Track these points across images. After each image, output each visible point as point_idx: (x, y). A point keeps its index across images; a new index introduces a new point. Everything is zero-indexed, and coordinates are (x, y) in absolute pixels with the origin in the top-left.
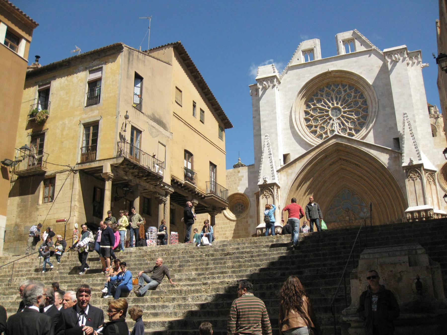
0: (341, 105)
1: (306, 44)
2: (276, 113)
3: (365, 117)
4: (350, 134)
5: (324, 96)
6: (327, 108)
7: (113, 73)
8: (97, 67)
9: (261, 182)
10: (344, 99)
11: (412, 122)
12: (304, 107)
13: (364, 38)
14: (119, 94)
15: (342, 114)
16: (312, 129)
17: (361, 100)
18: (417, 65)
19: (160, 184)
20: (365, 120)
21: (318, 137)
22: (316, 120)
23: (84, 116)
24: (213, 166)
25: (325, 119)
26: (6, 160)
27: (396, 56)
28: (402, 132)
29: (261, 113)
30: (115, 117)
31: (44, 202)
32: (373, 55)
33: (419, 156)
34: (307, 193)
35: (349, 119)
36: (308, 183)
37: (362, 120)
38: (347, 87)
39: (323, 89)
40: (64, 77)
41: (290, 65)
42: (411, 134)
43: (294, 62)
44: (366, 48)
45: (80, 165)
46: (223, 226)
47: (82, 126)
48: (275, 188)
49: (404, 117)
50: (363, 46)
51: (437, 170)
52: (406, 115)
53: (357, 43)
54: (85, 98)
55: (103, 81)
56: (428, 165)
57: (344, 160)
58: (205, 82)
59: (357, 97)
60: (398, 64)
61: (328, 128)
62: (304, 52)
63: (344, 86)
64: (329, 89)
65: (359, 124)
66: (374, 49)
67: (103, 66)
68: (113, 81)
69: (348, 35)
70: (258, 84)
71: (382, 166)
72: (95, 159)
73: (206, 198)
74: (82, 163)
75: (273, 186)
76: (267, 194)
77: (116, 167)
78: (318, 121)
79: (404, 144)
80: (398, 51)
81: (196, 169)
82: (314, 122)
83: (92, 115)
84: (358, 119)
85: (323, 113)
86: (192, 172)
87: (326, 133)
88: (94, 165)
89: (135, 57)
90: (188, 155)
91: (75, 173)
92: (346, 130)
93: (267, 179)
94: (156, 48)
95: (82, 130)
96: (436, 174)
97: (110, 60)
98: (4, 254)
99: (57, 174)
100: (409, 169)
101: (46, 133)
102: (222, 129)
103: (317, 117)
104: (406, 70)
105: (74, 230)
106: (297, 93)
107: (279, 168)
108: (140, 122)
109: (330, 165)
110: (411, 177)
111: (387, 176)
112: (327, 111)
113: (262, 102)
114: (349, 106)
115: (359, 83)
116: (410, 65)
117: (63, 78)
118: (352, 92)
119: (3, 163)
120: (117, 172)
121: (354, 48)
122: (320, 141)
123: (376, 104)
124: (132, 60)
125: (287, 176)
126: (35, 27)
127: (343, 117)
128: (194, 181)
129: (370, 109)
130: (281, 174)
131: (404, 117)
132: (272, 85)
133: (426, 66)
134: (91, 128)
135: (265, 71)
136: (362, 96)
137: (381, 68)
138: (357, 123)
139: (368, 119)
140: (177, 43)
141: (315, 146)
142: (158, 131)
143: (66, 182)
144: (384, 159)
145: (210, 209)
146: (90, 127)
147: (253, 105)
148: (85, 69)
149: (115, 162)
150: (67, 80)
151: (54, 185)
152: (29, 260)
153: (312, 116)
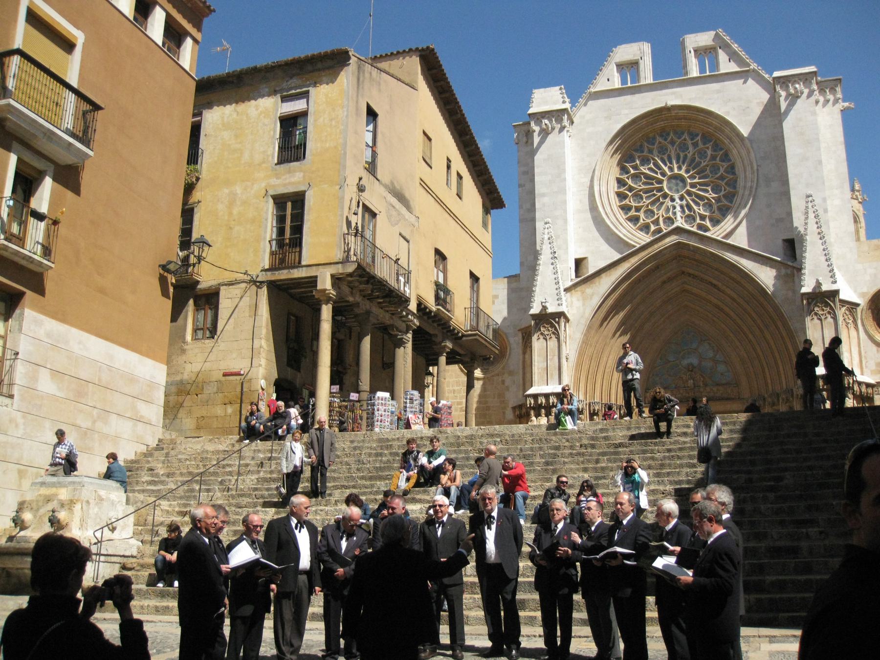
0: (687, 171)
1: (625, 52)
2: (565, 179)
3: (730, 197)
4: (700, 227)
5: (655, 152)
6: (659, 176)
7: (329, 104)
8: (298, 91)
9: (535, 309)
10: (693, 160)
11: (821, 212)
12: (616, 172)
13: (735, 46)
14: (345, 144)
15: (688, 188)
16: (630, 214)
17: (725, 165)
18: (834, 104)
19: (402, 311)
20: (731, 202)
21: (641, 230)
22: (637, 196)
23: (274, 181)
24: (474, 278)
25: (654, 195)
26: (170, 262)
27: (797, 86)
28: (801, 229)
29: (537, 179)
30: (338, 187)
31: (195, 338)
32: (750, 81)
33: (833, 276)
34: (619, 333)
35: (701, 198)
36: (621, 315)
37: (725, 202)
38: (699, 138)
39: (654, 138)
40: (231, 104)
41: (593, 90)
42: (819, 233)
43: (601, 84)
44: (739, 66)
45: (269, 273)
46: (456, 388)
47: (271, 201)
48: (562, 320)
49: (807, 202)
50: (732, 63)
51: (862, 301)
52: (810, 199)
53: (722, 56)
54: (274, 148)
55: (311, 119)
56: (847, 294)
57: (690, 275)
58: (467, 123)
59: (718, 159)
60: (799, 101)
61: (660, 214)
62: (620, 66)
63: (693, 136)
64: (666, 140)
65: (719, 209)
66: (754, 70)
67: (310, 89)
68: (331, 120)
69: (705, 39)
70: (532, 124)
71: (762, 291)
72: (300, 262)
73: (464, 338)
74: (271, 269)
75: (559, 318)
76: (546, 333)
77: (338, 279)
78: (642, 199)
79: (805, 252)
80: (801, 77)
81: (451, 285)
82: (634, 201)
83: (291, 179)
84: (718, 200)
85: (652, 184)
86: (447, 292)
87: (656, 222)
88: (297, 273)
89: (367, 75)
90: (440, 256)
91: (258, 287)
92: (694, 219)
93: (547, 305)
94: (386, 55)
95: (270, 207)
96: (859, 309)
97: (324, 78)
98: (163, 433)
99: (222, 288)
100: (813, 299)
101: (195, 210)
102: (486, 210)
103: (640, 191)
104: (814, 113)
105: (260, 391)
106: (605, 144)
107: (569, 284)
108: (376, 197)
109: (664, 282)
110: (816, 314)
111: (771, 310)
112: (660, 182)
113: (539, 158)
114: (701, 173)
115: (722, 131)
116: (821, 104)
117: (228, 107)
118: (708, 148)
119: (164, 267)
120: (339, 288)
121: (715, 65)
122: (646, 239)
123: (753, 173)
124: (363, 81)
125: (584, 299)
126: (207, 15)
127: (689, 193)
128: (448, 306)
129: (741, 183)
130: (571, 296)
131: (807, 202)
132: (559, 126)
133: (848, 108)
134: (289, 205)
135: (547, 98)
136: (726, 157)
137: (766, 105)
138: (715, 207)
139: (737, 200)
140: (428, 48)
141: (638, 246)
142: (399, 214)
143: (241, 304)
144: (766, 277)
145: (467, 359)
146: (286, 203)
147: (518, 162)
148: (274, 93)
149: (340, 272)
150: (235, 110)
151: (216, 308)
152: (225, 445)
153: (631, 189)
